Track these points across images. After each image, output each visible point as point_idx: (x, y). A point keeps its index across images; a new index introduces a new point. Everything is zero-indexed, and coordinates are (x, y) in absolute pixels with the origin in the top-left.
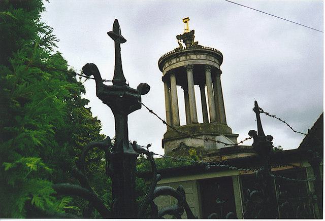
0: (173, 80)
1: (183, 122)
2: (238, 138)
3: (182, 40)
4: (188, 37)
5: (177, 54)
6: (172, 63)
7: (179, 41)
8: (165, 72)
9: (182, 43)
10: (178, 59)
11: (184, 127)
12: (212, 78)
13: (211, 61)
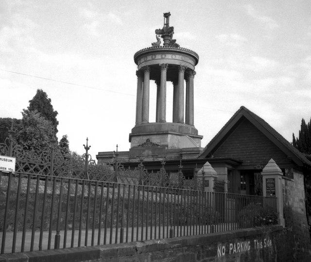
0: (147, 75)
1: (152, 118)
2: (202, 140)
4: (166, 32)
5: (153, 51)
6: (148, 59)
7: (158, 35)
8: (140, 67)
11: (152, 124)
13: (188, 62)
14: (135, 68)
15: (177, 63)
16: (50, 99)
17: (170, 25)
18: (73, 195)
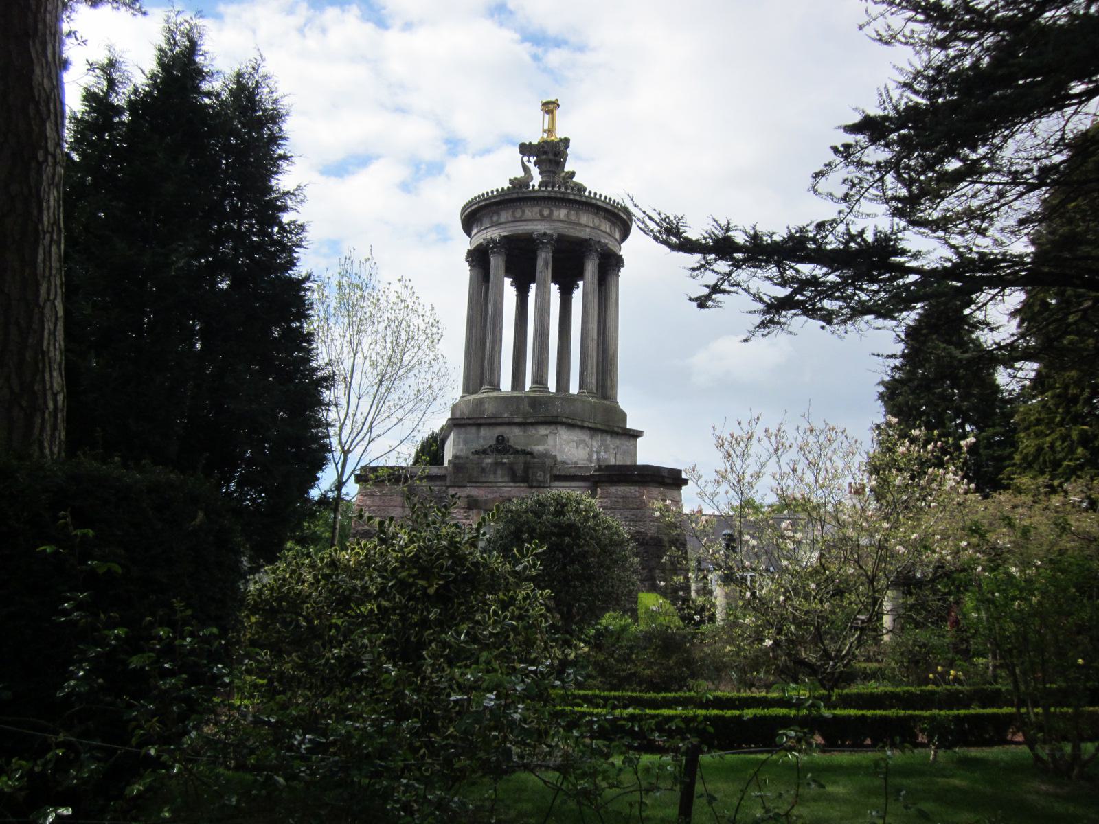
0: (497, 263)
3: (533, 159)
7: (526, 158)
9: (531, 166)
10: (495, 219)
12: (599, 272)
14: (464, 243)
15: (585, 234)
16: (511, 181)
17: (559, 134)
18: (308, 736)
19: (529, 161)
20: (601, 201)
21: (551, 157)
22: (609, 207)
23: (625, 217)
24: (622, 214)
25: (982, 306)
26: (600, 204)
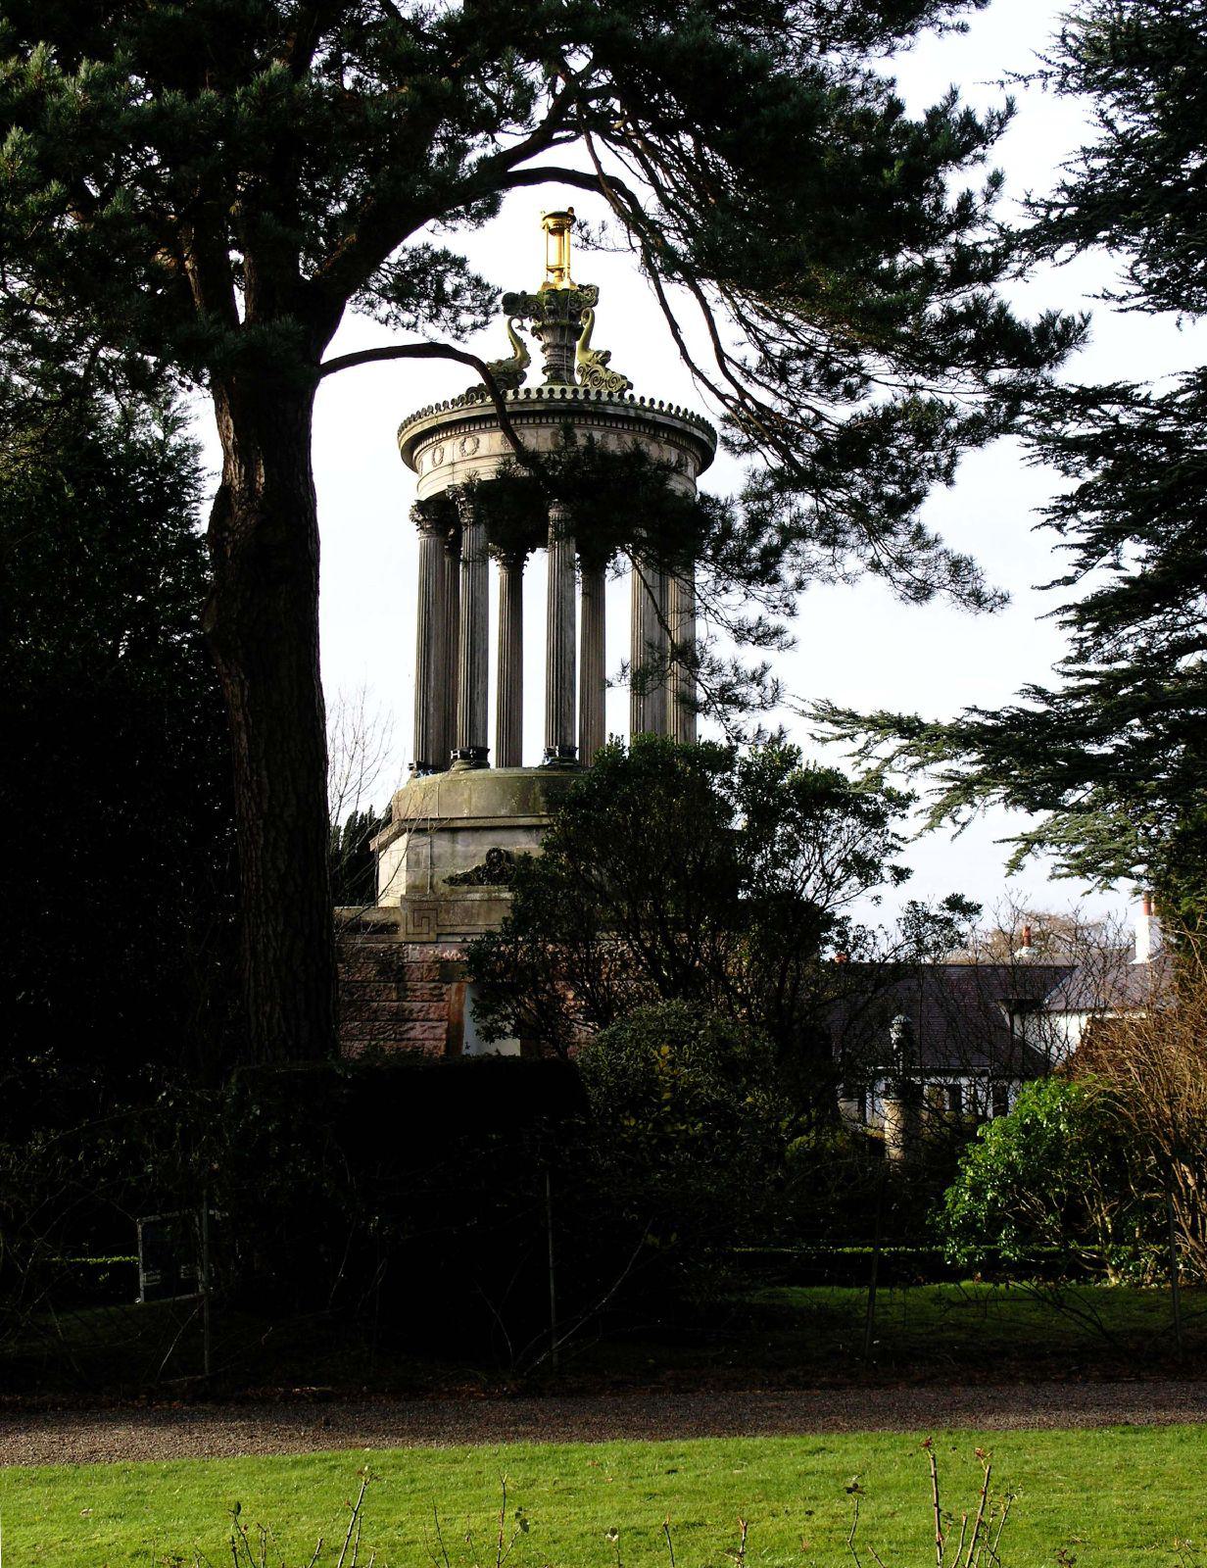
3: (529, 323)
7: (516, 323)
19: (522, 328)
20: (654, 411)
21: (566, 321)
22: (678, 424)
23: (705, 438)
24: (697, 433)
25: (824, 1004)
26: (661, 419)
